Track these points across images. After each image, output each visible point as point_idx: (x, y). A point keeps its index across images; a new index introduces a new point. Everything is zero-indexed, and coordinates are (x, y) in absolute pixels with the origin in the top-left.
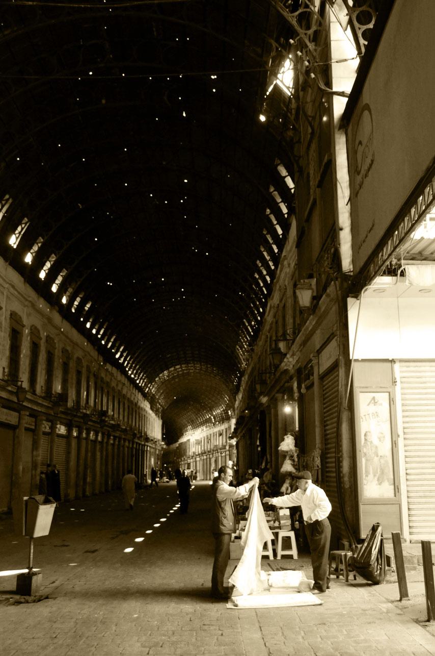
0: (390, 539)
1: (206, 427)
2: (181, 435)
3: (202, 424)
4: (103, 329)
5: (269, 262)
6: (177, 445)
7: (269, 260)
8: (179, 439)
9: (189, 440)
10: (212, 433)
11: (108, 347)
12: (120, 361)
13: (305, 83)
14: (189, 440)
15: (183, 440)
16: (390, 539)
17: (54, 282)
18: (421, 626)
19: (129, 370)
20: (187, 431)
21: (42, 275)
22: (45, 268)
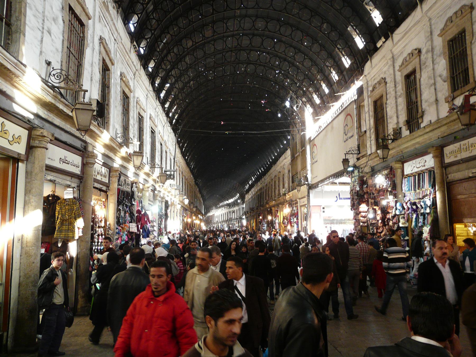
20: (212, 209)
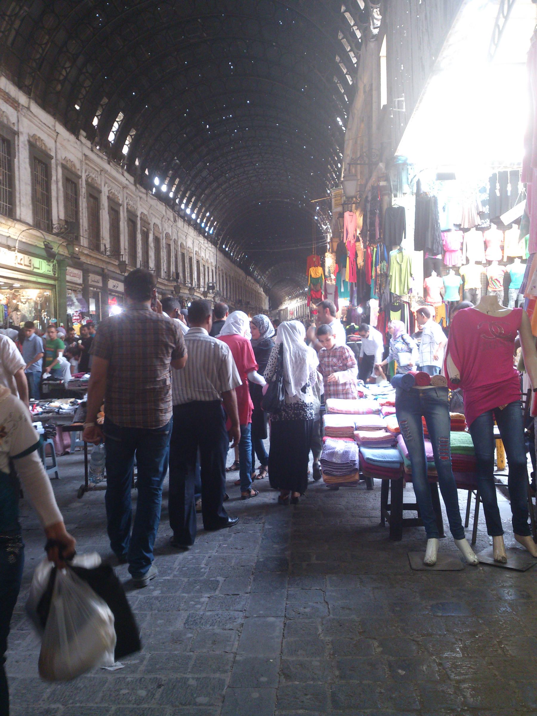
0: (392, 413)
1: (300, 299)
2: (281, 303)
3: (297, 297)
4: (186, 198)
5: (347, 76)
6: (278, 312)
7: (347, 74)
8: (279, 306)
9: (287, 308)
10: (304, 303)
11: (137, 160)
12: (476, 491)
13: (421, 58)
14: (287, 308)
15: (283, 307)
16: (392, 413)
17: (124, 144)
18: (517, 204)
19: (206, 225)
20: (285, 301)
21: (111, 137)
22: (127, 142)
